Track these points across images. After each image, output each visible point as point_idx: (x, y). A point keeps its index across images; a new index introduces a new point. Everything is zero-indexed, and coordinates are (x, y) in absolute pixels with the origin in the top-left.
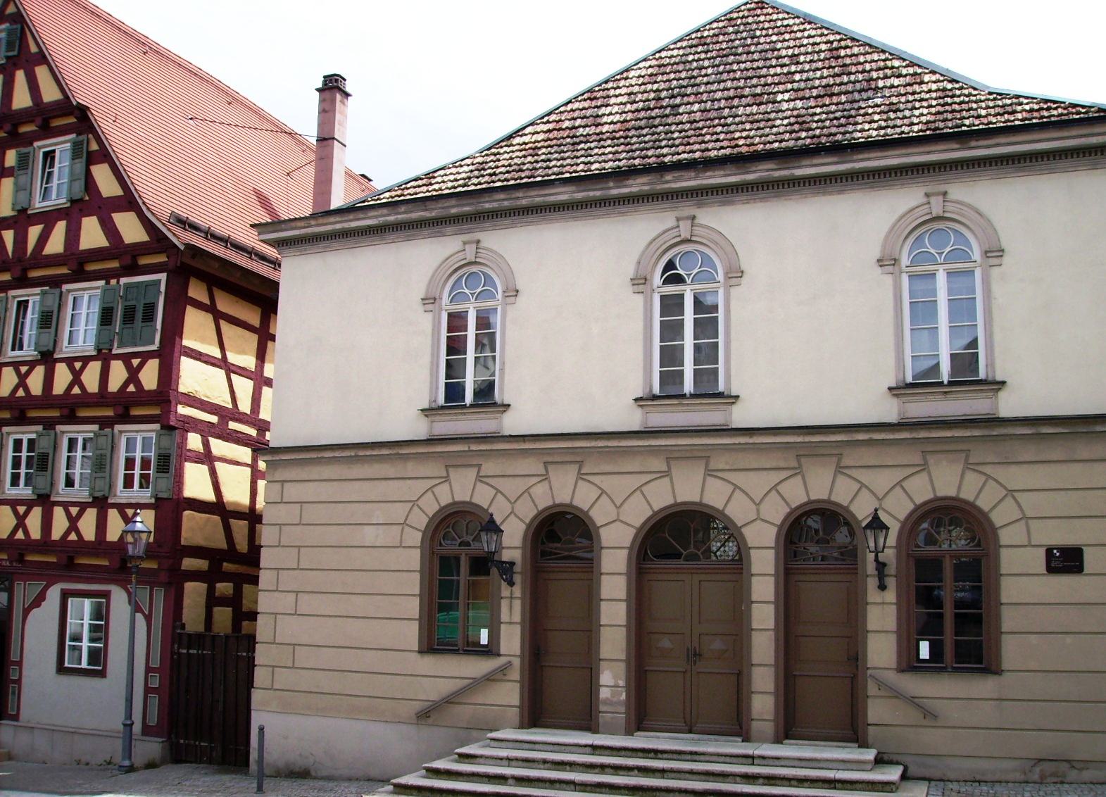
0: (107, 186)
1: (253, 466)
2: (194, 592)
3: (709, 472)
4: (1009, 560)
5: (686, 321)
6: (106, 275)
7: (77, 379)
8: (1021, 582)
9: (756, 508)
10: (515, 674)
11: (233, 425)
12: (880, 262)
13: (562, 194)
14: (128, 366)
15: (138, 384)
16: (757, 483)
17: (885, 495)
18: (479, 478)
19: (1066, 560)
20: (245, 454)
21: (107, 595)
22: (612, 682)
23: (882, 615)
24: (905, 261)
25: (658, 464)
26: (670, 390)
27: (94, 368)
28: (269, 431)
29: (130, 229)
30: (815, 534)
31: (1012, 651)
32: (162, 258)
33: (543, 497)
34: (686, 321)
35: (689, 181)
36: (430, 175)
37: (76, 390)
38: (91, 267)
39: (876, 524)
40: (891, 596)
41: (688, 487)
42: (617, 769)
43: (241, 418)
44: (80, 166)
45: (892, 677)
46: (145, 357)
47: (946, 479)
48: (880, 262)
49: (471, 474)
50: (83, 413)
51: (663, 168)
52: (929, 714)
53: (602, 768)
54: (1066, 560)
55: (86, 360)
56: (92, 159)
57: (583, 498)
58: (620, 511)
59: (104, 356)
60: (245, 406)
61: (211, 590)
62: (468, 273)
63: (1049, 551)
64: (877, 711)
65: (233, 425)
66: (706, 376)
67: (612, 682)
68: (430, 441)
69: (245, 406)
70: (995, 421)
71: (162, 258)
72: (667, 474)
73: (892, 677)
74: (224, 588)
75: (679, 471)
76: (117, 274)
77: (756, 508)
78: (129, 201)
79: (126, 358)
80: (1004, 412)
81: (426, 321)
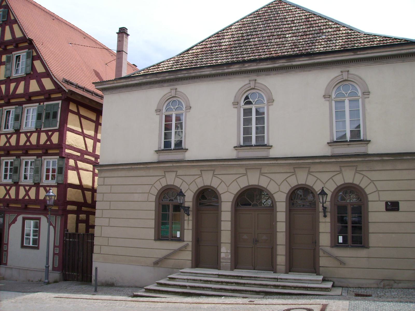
0: (40, 68)
1: (93, 172)
2: (72, 218)
3: (261, 174)
4: (372, 206)
5: (253, 118)
6: (39, 101)
7: (28, 140)
8: (376, 214)
9: (279, 187)
10: (190, 248)
11: (86, 157)
12: (324, 96)
13: (207, 72)
14: (47, 135)
15: (51, 141)
16: (279, 178)
17: (326, 182)
18: (177, 176)
19: (393, 206)
20: (90, 167)
21: (39, 219)
22: (225, 251)
23: (325, 226)
24: (333, 96)
25: (242, 171)
26: (247, 143)
27: (35, 135)
28: (99, 158)
29: (48, 84)
30: (300, 196)
31: (373, 240)
32: (60, 95)
33: (200, 183)
34: (253, 118)
35: (254, 67)
36: (158, 64)
37: (28, 144)
38: (33, 98)
39: (323, 193)
40: (328, 219)
41: (253, 179)
42: (227, 283)
43: (89, 154)
44: (29, 61)
45: (329, 249)
46: (54, 131)
47: (348, 176)
48: (324, 96)
49: (174, 174)
50: (30, 152)
51: (244, 62)
52: (342, 263)
53: (222, 283)
54: (393, 206)
55: (32, 132)
56: (34, 59)
57: (215, 183)
58: (228, 188)
59: (38, 131)
60: (90, 149)
61: (78, 217)
62: (173, 100)
63: (387, 203)
64: (323, 262)
65: (86, 157)
66: (179, 144)
67: (225, 251)
68: (159, 162)
69: (90, 149)
70: (366, 155)
71: (60, 95)
72: (246, 174)
73: (329, 249)
74: (83, 216)
75: (250, 173)
76: (43, 101)
77: (279, 187)
78: (48, 74)
79: (47, 132)
80: (370, 152)
81: (157, 118)
